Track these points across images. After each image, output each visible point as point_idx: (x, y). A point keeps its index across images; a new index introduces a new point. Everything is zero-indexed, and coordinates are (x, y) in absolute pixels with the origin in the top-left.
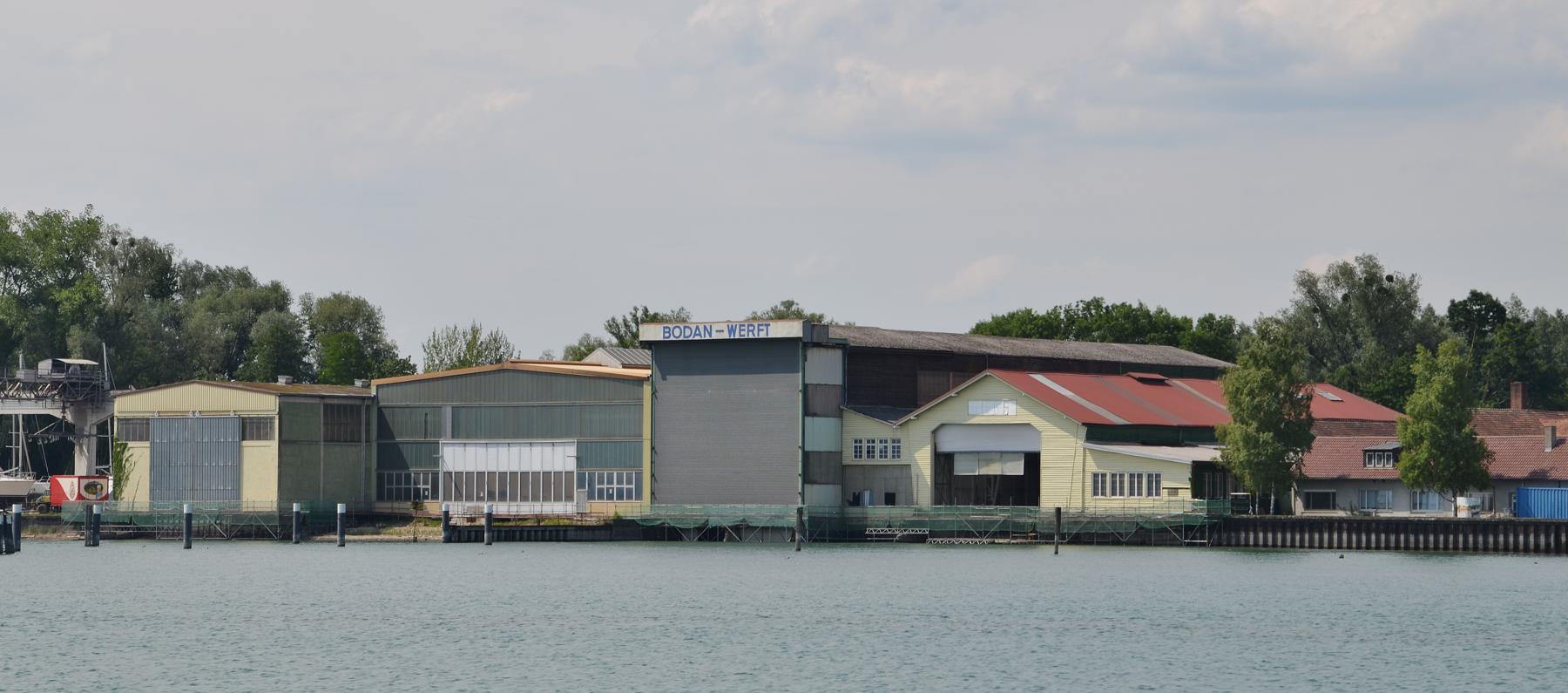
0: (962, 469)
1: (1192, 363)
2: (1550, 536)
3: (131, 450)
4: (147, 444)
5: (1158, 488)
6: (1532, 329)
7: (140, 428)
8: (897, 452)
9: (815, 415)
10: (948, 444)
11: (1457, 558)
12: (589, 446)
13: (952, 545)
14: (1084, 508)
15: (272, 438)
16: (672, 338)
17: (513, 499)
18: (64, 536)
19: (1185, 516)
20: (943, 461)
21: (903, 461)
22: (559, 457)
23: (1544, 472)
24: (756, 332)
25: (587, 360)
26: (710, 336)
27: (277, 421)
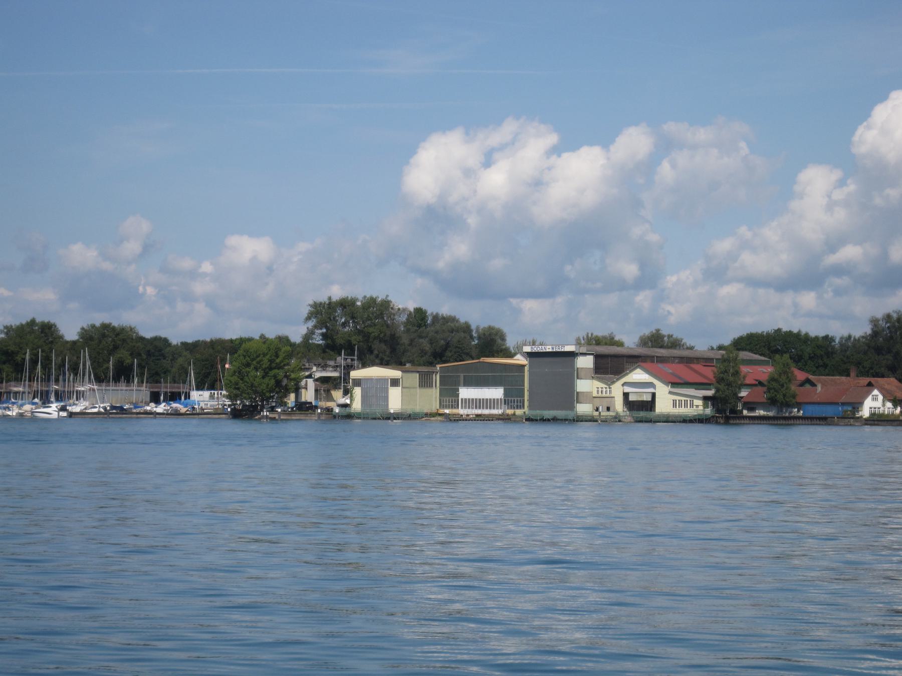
0: (632, 398)
1: (760, 359)
4: (360, 388)
5: (693, 405)
6: (286, 367)
7: (358, 382)
8: (610, 392)
9: (581, 379)
10: (627, 389)
11: (411, 421)
13: (793, 425)
15: (400, 386)
18: (813, 422)
19: (699, 415)
20: (626, 395)
21: (612, 395)
22: (497, 393)
25: (515, 358)
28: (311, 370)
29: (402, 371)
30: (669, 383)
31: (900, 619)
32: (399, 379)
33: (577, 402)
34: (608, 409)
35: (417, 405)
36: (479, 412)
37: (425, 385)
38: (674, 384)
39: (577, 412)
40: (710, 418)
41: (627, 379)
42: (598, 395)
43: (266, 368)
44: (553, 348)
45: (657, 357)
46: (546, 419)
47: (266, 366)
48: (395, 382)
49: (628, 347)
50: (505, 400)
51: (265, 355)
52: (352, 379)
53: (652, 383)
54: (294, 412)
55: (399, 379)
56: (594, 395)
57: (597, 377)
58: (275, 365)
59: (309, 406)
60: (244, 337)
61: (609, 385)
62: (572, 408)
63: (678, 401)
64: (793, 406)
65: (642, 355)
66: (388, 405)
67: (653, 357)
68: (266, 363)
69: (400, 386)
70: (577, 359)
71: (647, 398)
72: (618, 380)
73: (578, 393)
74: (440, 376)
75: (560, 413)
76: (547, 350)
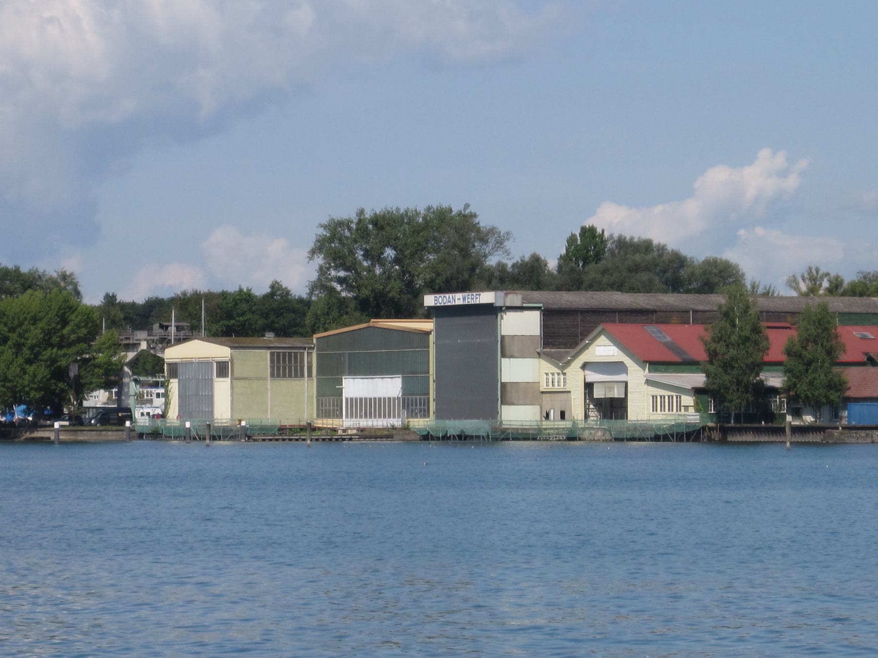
0: (598, 393)
2: (68, 600)
3: (172, 384)
7: (174, 369)
9: (512, 357)
10: (592, 377)
12: (221, 364)
14: (373, 425)
16: (438, 305)
17: (389, 417)
20: (589, 387)
23: (503, 319)
24: (451, 297)
26: (455, 303)
27: (230, 363)
28: (137, 348)
29: (232, 348)
30: (645, 362)
31: (1, 589)
32: (228, 362)
33: (502, 403)
34: (563, 415)
35: (267, 412)
36: (364, 423)
37: (173, 376)
38: (655, 365)
39: (501, 422)
40: (699, 430)
41: (585, 357)
42: (550, 388)
43: (36, 345)
44: (464, 299)
45: (695, 312)
46: (450, 436)
47: (34, 341)
48: (223, 369)
49: (110, 300)
50: (404, 400)
51: (35, 320)
52: (169, 364)
53: (622, 363)
54: (92, 428)
55: (228, 362)
56: (542, 389)
57: (545, 353)
58: (58, 339)
59: (122, 416)
60: (232, 292)
61: (562, 368)
62: (493, 413)
63: (659, 398)
64: (80, 360)
65: (657, 309)
66: (212, 412)
67: (687, 312)
68: (35, 334)
69: (228, 377)
70: (502, 318)
71: (619, 394)
72: (575, 357)
73: (504, 385)
74: (317, 354)
75: (470, 425)
76: (458, 303)
